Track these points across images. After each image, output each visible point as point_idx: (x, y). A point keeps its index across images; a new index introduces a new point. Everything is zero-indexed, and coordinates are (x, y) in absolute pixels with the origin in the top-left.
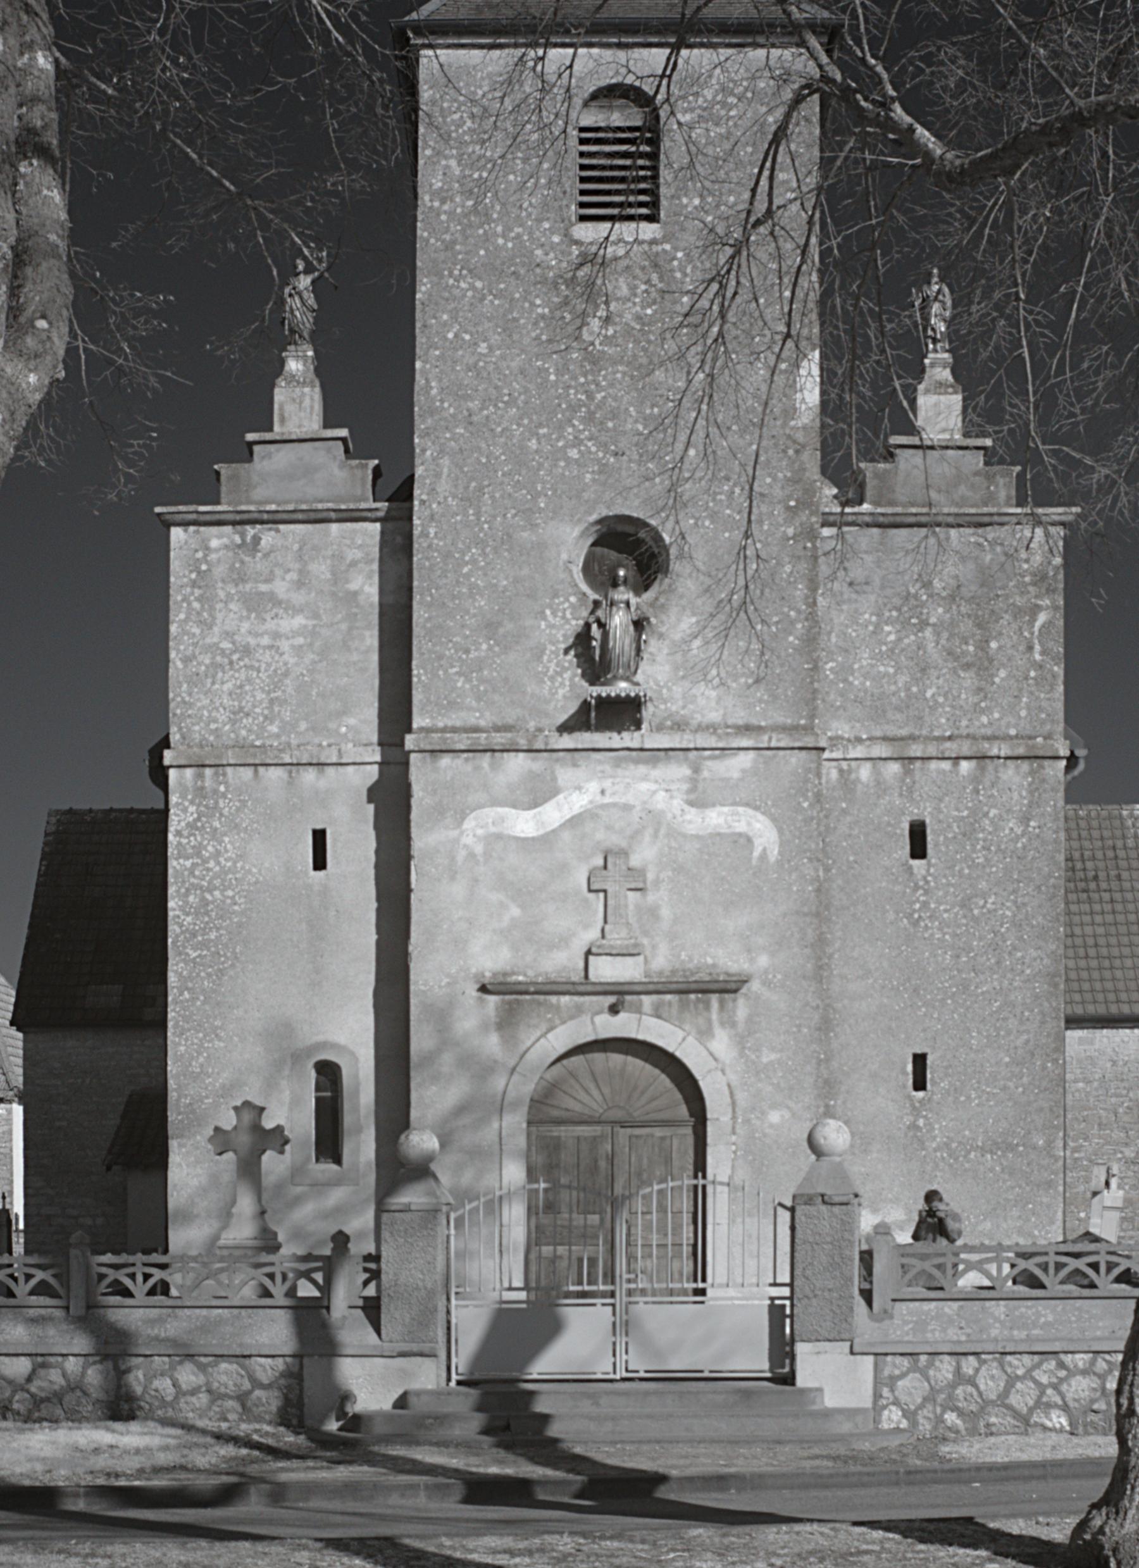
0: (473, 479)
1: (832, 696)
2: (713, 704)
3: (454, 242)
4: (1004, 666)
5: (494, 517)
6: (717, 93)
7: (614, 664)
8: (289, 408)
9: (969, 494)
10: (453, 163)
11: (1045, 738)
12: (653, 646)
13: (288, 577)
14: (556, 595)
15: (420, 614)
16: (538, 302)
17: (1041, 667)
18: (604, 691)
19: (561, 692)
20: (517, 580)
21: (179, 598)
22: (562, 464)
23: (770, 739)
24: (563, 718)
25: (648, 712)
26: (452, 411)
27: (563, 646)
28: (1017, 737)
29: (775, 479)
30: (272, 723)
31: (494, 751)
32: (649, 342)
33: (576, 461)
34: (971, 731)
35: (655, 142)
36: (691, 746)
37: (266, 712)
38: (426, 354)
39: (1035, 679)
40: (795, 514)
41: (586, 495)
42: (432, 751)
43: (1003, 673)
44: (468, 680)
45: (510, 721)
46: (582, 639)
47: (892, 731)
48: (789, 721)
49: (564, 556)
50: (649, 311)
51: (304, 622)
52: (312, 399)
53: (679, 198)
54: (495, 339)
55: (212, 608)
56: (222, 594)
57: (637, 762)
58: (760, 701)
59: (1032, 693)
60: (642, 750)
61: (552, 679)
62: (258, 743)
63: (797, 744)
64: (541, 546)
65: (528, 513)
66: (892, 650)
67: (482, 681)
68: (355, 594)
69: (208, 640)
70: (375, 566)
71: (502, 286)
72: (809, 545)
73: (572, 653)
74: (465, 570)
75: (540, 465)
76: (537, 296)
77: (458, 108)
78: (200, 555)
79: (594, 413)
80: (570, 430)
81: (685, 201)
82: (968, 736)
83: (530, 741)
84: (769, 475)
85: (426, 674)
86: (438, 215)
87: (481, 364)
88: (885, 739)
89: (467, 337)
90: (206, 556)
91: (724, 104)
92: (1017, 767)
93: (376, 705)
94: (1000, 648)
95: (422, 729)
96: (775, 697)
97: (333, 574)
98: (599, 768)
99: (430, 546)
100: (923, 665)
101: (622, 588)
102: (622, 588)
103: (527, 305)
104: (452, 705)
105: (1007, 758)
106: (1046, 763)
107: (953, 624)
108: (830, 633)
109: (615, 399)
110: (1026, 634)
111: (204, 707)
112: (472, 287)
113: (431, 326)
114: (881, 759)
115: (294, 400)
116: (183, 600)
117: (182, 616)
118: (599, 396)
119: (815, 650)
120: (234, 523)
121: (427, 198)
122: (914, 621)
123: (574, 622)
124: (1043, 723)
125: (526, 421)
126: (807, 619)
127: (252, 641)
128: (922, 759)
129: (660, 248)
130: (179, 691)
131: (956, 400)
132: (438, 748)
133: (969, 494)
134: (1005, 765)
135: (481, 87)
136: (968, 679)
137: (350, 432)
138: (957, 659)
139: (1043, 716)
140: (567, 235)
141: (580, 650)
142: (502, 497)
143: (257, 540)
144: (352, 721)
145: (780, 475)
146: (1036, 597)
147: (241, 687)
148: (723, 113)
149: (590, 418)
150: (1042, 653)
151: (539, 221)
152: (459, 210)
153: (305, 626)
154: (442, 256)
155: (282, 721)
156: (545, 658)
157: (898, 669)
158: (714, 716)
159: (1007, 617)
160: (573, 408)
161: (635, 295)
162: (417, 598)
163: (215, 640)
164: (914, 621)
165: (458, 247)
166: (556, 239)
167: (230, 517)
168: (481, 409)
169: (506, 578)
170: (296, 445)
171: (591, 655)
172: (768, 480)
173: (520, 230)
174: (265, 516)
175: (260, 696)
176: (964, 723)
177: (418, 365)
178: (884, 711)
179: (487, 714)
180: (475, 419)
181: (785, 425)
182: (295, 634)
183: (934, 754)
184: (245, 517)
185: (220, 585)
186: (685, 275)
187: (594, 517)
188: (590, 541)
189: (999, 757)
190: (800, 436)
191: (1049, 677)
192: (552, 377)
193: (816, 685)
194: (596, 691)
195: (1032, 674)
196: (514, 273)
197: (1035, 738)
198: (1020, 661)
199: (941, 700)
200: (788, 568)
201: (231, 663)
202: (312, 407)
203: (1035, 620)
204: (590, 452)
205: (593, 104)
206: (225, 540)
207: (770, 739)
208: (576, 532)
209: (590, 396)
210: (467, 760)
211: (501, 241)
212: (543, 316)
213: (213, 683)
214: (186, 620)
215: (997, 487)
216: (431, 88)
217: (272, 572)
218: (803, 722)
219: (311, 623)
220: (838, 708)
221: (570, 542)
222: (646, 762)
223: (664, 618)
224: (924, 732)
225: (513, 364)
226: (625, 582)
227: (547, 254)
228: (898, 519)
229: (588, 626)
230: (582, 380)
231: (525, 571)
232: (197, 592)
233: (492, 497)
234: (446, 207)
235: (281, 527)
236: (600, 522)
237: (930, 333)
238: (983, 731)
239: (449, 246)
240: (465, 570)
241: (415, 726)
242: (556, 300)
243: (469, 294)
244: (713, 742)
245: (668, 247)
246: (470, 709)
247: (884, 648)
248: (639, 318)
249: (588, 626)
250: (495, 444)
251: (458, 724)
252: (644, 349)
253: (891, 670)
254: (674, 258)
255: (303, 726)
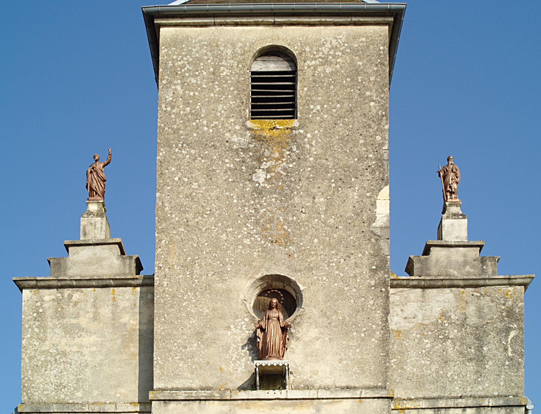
0: (188, 256)
1: (395, 377)
2: (328, 375)
3: (179, 129)
4: (491, 359)
5: (201, 275)
6: (330, 49)
7: (270, 350)
8: (89, 228)
9: (472, 270)
10: (179, 87)
11: (514, 396)
12: (292, 344)
13: (87, 316)
14: (237, 318)
15: (158, 328)
16: (227, 161)
17: (512, 359)
18: (263, 363)
19: (239, 369)
20: (214, 310)
21: (27, 326)
22: (241, 247)
23: (361, 392)
24: (240, 383)
25: (290, 379)
26: (177, 219)
27: (241, 345)
28: (498, 396)
29: (364, 254)
30: (78, 391)
31: (200, 400)
32: (291, 182)
33: (249, 245)
34: (472, 393)
35: (294, 80)
36: (315, 397)
37: (75, 386)
38: (162, 189)
39: (508, 365)
40: (375, 273)
41: (254, 264)
42: (164, 400)
43: (490, 363)
44: (186, 363)
45: (211, 385)
46: (252, 341)
47: (428, 394)
48: (372, 384)
49: (242, 297)
50: (291, 166)
51: (96, 339)
52: (102, 223)
53: (308, 105)
54: (202, 181)
55: (45, 332)
56: (50, 324)
57: (283, 406)
58: (355, 373)
59: (506, 373)
60: (286, 399)
61: (234, 362)
62: (70, 402)
63: (376, 396)
64: (229, 291)
65: (221, 274)
66: (429, 352)
67: (194, 363)
68: (125, 324)
69: (43, 348)
70: (137, 310)
71: (206, 152)
72: (383, 290)
73: (247, 348)
74: (184, 304)
75: (228, 248)
76: (227, 158)
77: (182, 59)
78: (38, 304)
79: (259, 220)
80: (245, 229)
81: (312, 107)
82: (471, 396)
83: (221, 395)
84: (361, 252)
85: (161, 359)
86: (170, 115)
87: (194, 194)
88: (424, 398)
89: (186, 180)
90: (42, 304)
91: (334, 56)
92: (498, 411)
93: (137, 382)
94: (489, 350)
95: (159, 389)
96: (364, 372)
97: (113, 314)
98: (261, 409)
99: (164, 291)
100: (446, 359)
101: (275, 310)
102: (275, 310)
103: (220, 162)
104: (177, 376)
105: (492, 407)
106: (514, 409)
107: (463, 338)
108: (393, 344)
109: (271, 212)
110: (503, 342)
111: (40, 383)
112: (189, 153)
113: (166, 173)
114: (422, 408)
115: (92, 224)
116: (29, 328)
117: (29, 336)
118: (262, 211)
119: (387, 346)
120: (58, 287)
121: (163, 106)
122: (441, 337)
123: (247, 332)
124: (513, 388)
125: (220, 225)
126: (382, 329)
127: (68, 349)
128: (446, 408)
129: (297, 132)
130: (27, 374)
131: (464, 222)
132: (168, 398)
133: (472, 270)
134: (491, 411)
135: (194, 47)
136: (471, 366)
137: (122, 239)
138: (465, 356)
139: (513, 385)
140: (244, 125)
141: (250, 346)
142: (206, 265)
143: (70, 296)
144: (123, 391)
145: (367, 253)
146: (509, 323)
147: (61, 372)
148: (333, 60)
149: (257, 222)
150: (513, 352)
151: (228, 117)
152: (182, 112)
153: (97, 341)
154: (172, 137)
155: (84, 390)
156: (230, 351)
157: (432, 362)
158: (328, 382)
159: (492, 334)
160: (247, 217)
161: (283, 157)
162: (156, 319)
163: (47, 348)
164: (441, 337)
165: (181, 132)
166: (237, 127)
167: (55, 283)
168: (194, 218)
169: (208, 308)
170: (92, 247)
171: (257, 347)
172: (360, 255)
173: (217, 123)
174: (74, 283)
175: (71, 377)
176: (469, 389)
177: (158, 195)
178: (424, 384)
179: (197, 381)
180: (190, 223)
181: (370, 224)
182: (92, 345)
183: (452, 406)
184: (63, 283)
185: (49, 319)
186: (312, 146)
187: (259, 276)
188: (257, 291)
189: (488, 407)
190: (378, 232)
191: (516, 364)
192: (235, 201)
193: (387, 364)
194: (259, 363)
195: (507, 363)
196: (213, 145)
197: (509, 396)
198: (500, 356)
199: (456, 377)
200: (372, 302)
201: (56, 360)
202: (101, 228)
203: (509, 335)
204: (257, 241)
205: (258, 59)
206: (53, 297)
207: (361, 392)
208: (249, 283)
209: (256, 210)
210: (185, 405)
211: (206, 129)
212: (230, 169)
213: (45, 371)
214: (31, 338)
215: (487, 266)
216: (166, 48)
217: (78, 313)
218: (380, 384)
219: (100, 339)
220: (398, 383)
221: (246, 291)
222: (289, 406)
223: (299, 329)
224: (446, 395)
225: (212, 194)
226: (276, 307)
227: (232, 136)
228: (432, 283)
229: (255, 332)
230: (252, 202)
231: (219, 305)
232: (37, 323)
233: (200, 265)
234: (174, 111)
235: (83, 289)
236: (262, 279)
237: (448, 189)
238: (479, 393)
239: (176, 131)
240: (184, 304)
241: (155, 387)
242: (237, 160)
243: (188, 156)
244: (327, 394)
245: (302, 131)
246: (186, 378)
247: (424, 351)
248: (285, 169)
249: (255, 332)
250: (201, 237)
251: (180, 386)
252: (289, 186)
253: (428, 363)
254: (306, 137)
255: (96, 393)
